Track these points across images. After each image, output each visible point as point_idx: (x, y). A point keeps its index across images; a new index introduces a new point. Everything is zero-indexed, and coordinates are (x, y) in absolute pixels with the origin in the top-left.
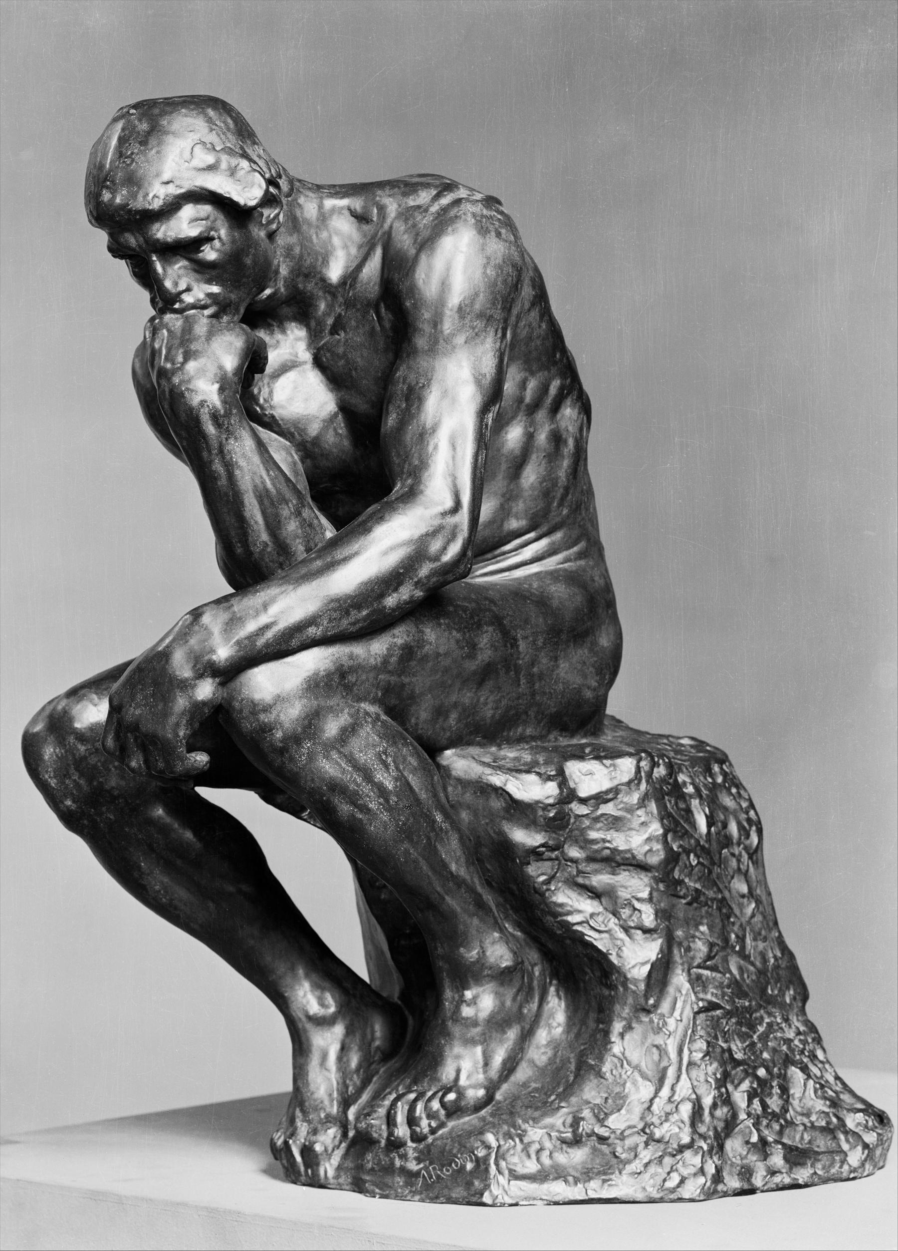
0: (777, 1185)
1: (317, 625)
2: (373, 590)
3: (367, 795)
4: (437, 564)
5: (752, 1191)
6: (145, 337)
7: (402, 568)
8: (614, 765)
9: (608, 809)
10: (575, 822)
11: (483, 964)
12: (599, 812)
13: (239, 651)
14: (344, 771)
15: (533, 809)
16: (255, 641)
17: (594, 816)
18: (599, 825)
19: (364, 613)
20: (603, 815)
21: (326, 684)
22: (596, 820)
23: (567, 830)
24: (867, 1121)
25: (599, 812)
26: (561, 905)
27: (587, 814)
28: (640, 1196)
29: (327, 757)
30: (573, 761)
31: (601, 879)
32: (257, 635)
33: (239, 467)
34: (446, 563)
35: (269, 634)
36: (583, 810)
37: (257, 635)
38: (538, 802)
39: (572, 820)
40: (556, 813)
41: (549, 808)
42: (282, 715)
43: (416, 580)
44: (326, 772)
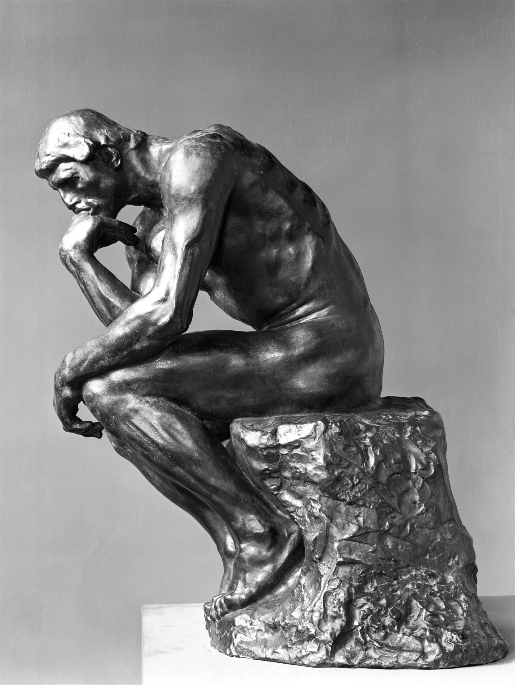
0: (368, 665)
1: (104, 360)
2: (124, 342)
3: (147, 443)
4: (156, 327)
5: (352, 666)
6: (79, 222)
7: (138, 330)
8: (301, 427)
9: (297, 451)
10: (282, 458)
11: (245, 531)
12: (293, 452)
13: (73, 373)
14: (133, 431)
15: (256, 450)
16: (79, 369)
17: (290, 454)
18: (294, 460)
19: (125, 353)
20: (295, 454)
21: (119, 388)
22: (292, 456)
23: (279, 462)
24: (453, 637)
25: (293, 452)
26: (285, 501)
27: (287, 454)
28: (287, 659)
29: (124, 424)
30: (283, 425)
31: (300, 488)
32: (80, 365)
33: (157, 279)
34: (160, 326)
35: (85, 364)
36: (284, 451)
37: (80, 365)
38: (257, 447)
39: (281, 457)
40: (267, 453)
41: (263, 450)
42: (98, 403)
43: (147, 335)
44: (125, 431)
